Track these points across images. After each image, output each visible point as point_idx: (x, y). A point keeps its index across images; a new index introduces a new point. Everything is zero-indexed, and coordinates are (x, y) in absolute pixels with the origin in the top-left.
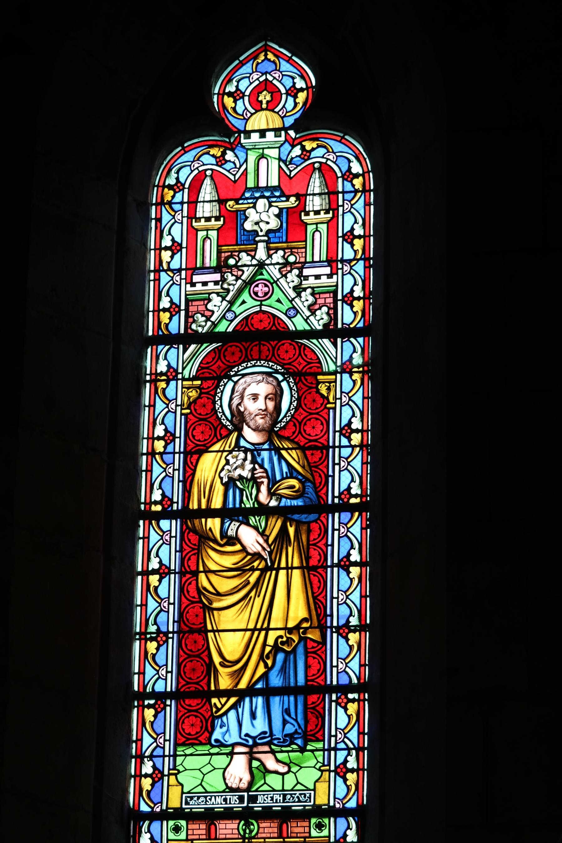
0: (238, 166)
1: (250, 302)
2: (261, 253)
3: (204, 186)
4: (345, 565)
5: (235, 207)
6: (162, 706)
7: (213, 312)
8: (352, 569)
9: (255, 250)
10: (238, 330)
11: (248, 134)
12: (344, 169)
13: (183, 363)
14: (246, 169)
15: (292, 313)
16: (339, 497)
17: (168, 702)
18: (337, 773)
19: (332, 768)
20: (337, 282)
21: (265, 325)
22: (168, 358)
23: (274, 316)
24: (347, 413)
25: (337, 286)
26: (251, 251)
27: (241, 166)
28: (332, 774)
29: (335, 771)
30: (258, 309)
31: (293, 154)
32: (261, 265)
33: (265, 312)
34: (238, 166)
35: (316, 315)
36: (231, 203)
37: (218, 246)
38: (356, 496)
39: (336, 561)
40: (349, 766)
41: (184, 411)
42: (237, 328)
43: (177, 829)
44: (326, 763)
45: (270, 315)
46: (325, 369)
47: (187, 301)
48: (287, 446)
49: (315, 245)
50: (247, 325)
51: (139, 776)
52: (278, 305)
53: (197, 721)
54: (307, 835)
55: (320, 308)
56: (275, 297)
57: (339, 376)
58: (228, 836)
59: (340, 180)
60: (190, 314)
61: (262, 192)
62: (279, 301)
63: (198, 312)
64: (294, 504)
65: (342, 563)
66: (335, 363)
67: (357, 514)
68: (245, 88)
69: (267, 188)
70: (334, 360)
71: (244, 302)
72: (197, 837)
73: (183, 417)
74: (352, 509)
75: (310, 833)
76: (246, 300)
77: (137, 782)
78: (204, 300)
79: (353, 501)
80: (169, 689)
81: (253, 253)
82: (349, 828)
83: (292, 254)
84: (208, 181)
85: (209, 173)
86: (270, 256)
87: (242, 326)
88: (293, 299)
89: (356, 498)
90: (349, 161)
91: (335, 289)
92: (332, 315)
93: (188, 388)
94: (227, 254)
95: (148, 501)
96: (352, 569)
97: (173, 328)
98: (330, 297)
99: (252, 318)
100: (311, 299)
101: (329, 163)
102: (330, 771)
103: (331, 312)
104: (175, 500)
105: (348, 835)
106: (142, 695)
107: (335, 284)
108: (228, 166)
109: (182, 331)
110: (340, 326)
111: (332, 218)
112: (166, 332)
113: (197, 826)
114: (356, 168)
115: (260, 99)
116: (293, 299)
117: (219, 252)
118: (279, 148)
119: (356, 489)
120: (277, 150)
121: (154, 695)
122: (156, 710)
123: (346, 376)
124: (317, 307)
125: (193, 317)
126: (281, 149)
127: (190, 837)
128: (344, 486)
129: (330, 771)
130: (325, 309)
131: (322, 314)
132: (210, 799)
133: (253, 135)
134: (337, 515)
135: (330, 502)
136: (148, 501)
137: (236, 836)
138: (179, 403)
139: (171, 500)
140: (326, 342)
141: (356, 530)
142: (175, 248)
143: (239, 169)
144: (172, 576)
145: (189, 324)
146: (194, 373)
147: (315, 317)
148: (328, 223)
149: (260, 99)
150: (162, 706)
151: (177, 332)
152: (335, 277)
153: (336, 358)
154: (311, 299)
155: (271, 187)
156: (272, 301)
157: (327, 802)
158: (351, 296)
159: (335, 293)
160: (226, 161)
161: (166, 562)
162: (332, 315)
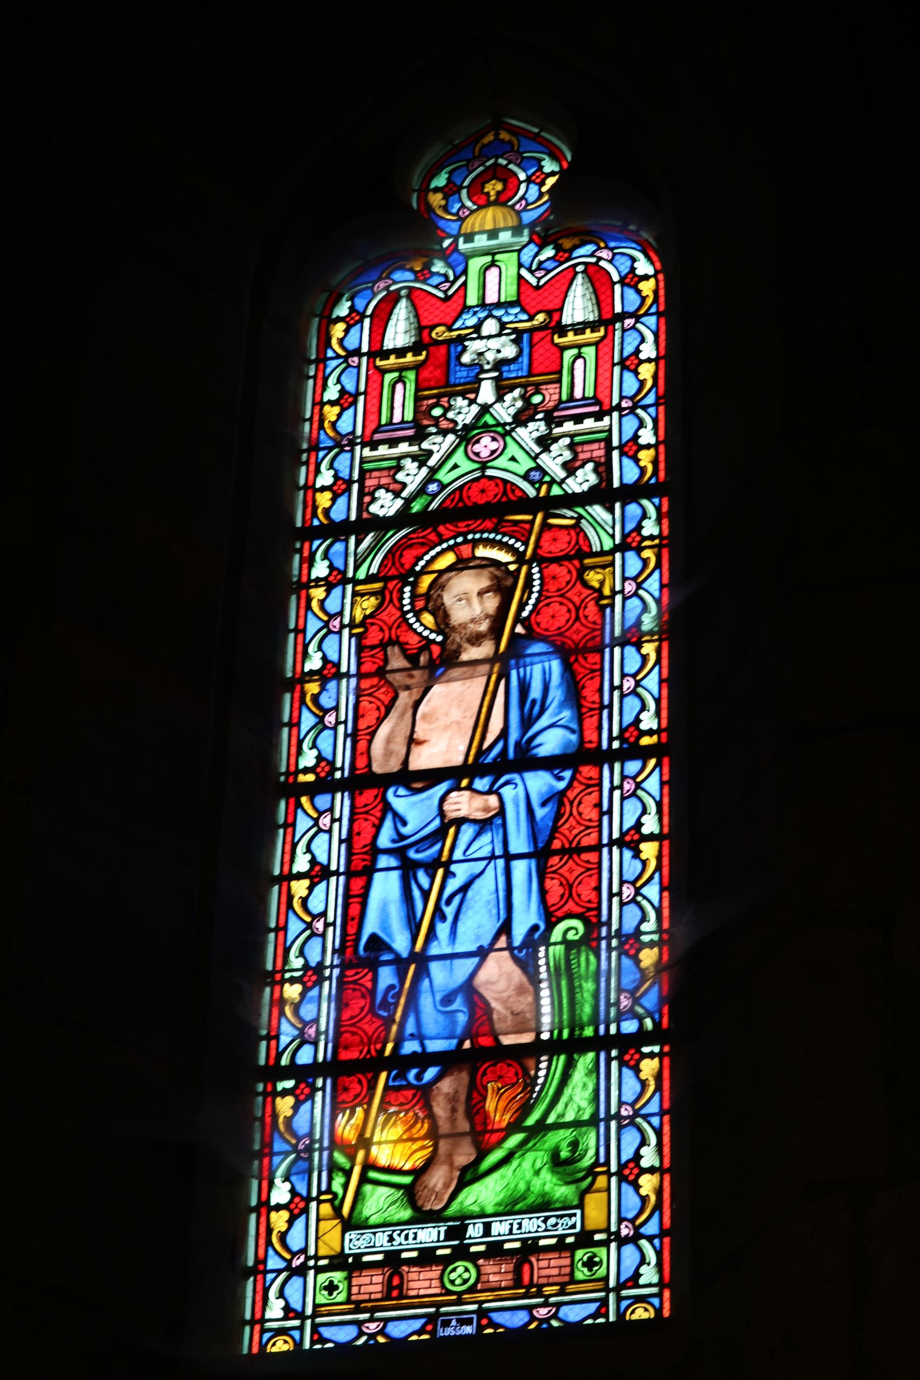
0: (452, 278)
1: (466, 466)
2: (487, 393)
3: (396, 311)
4: (632, 841)
5: (445, 334)
6: (307, 1091)
7: (404, 485)
8: (643, 846)
9: (477, 391)
10: (446, 508)
11: (469, 238)
12: (625, 270)
13: (355, 561)
14: (465, 284)
15: (536, 475)
16: (620, 737)
17: (319, 1083)
18: (622, 1178)
19: (614, 1168)
20: (611, 425)
21: (492, 494)
22: (330, 556)
23: (505, 482)
24: (632, 810)
25: (610, 430)
26: (471, 392)
27: (456, 278)
28: (614, 1180)
29: (620, 1174)
30: (477, 474)
31: (542, 257)
32: (485, 409)
33: (491, 478)
34: (452, 278)
35: (577, 477)
36: (440, 329)
37: (418, 389)
38: (650, 733)
39: (616, 835)
40: (645, 1163)
41: (355, 631)
42: (445, 505)
43: (331, 1288)
44: (602, 1160)
45: (497, 481)
46: (596, 547)
47: (362, 472)
48: (586, 511)
49: (583, 374)
50: (461, 499)
51: (265, 1207)
52: (512, 466)
53: (564, 576)
54: (567, 1279)
55: (582, 466)
56: (508, 454)
57: (618, 556)
58: (422, 1292)
59: (617, 288)
60: (367, 490)
61: (490, 311)
62: (513, 459)
63: (379, 487)
64: (435, 1185)
65: (628, 838)
66: (613, 536)
67: (652, 762)
68: (530, 259)
69: (499, 305)
70: (611, 531)
71: (456, 466)
72: (367, 1297)
73: (353, 640)
74: (644, 754)
75: (572, 1274)
76: (459, 464)
77: (263, 1219)
78: (389, 469)
79: (645, 741)
80: (320, 1058)
81: (472, 396)
82: (643, 1261)
83: (538, 392)
84: (403, 304)
85: (403, 292)
86: (500, 399)
87: (453, 500)
88: (537, 455)
89: (651, 736)
90: (634, 260)
91: (607, 436)
92: (604, 474)
93: (362, 595)
94: (431, 401)
95: (292, 769)
96: (643, 846)
97: (338, 514)
98: (599, 449)
99: (470, 488)
100: (568, 455)
101: (602, 264)
102: (609, 1175)
103: (602, 469)
104: (339, 764)
105: (642, 1157)
106: (275, 1072)
107: (607, 428)
108: (435, 280)
109: (353, 517)
110: (616, 484)
111: (603, 338)
112: (325, 522)
113: (367, 1280)
114: (644, 267)
115: (486, 190)
116: (537, 455)
117: (418, 399)
118: (519, 251)
119: (648, 721)
120: (516, 254)
121: (293, 1071)
122: (297, 1097)
123: (630, 650)
124: (578, 463)
125: (372, 494)
126: (601, 346)
127: (353, 1298)
128: (628, 719)
129: (609, 1175)
130: (590, 466)
131: (585, 474)
132: (539, 1227)
133: (477, 238)
134: (617, 766)
135: (605, 745)
136: (292, 769)
137: (438, 1291)
138: (346, 620)
139: (332, 763)
140: (598, 511)
141: (653, 784)
142: (346, 400)
143: (453, 283)
144: (333, 880)
145: (365, 505)
146: (374, 570)
147: (575, 479)
148: (597, 344)
149: (486, 190)
150: (307, 1091)
151: (343, 517)
152: (607, 419)
153: (613, 528)
154: (568, 455)
155: (505, 302)
156: (502, 462)
157: (603, 1225)
158: (634, 445)
159: (608, 440)
160: (433, 274)
161: (322, 858)
162: (604, 474)
